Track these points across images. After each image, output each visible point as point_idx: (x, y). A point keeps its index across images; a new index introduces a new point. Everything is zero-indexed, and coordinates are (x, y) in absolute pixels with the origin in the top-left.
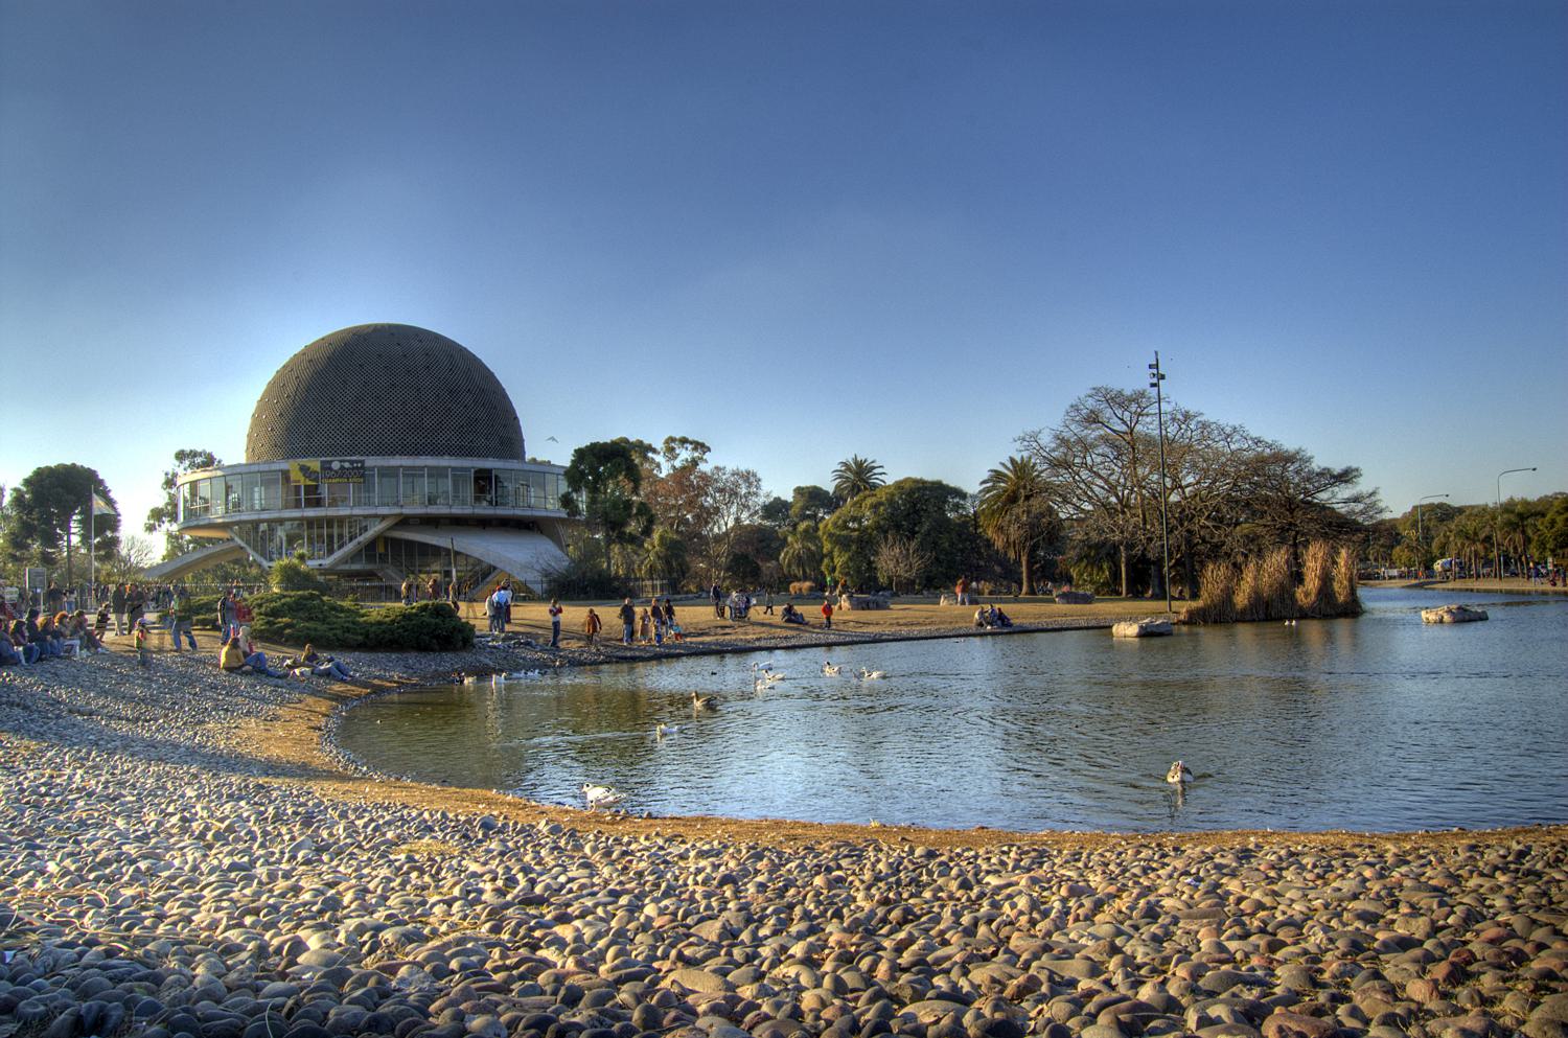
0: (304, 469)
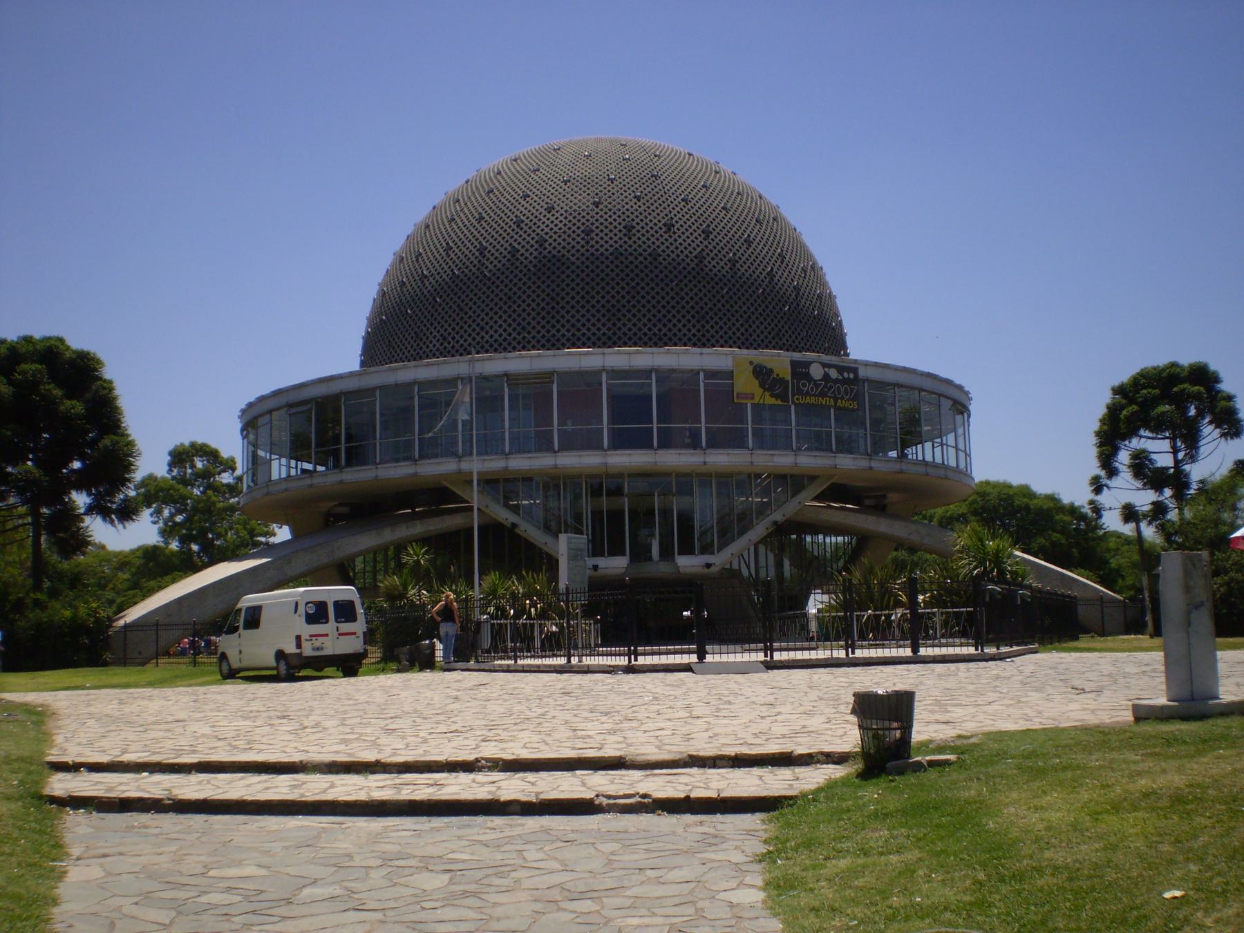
0: (761, 373)
